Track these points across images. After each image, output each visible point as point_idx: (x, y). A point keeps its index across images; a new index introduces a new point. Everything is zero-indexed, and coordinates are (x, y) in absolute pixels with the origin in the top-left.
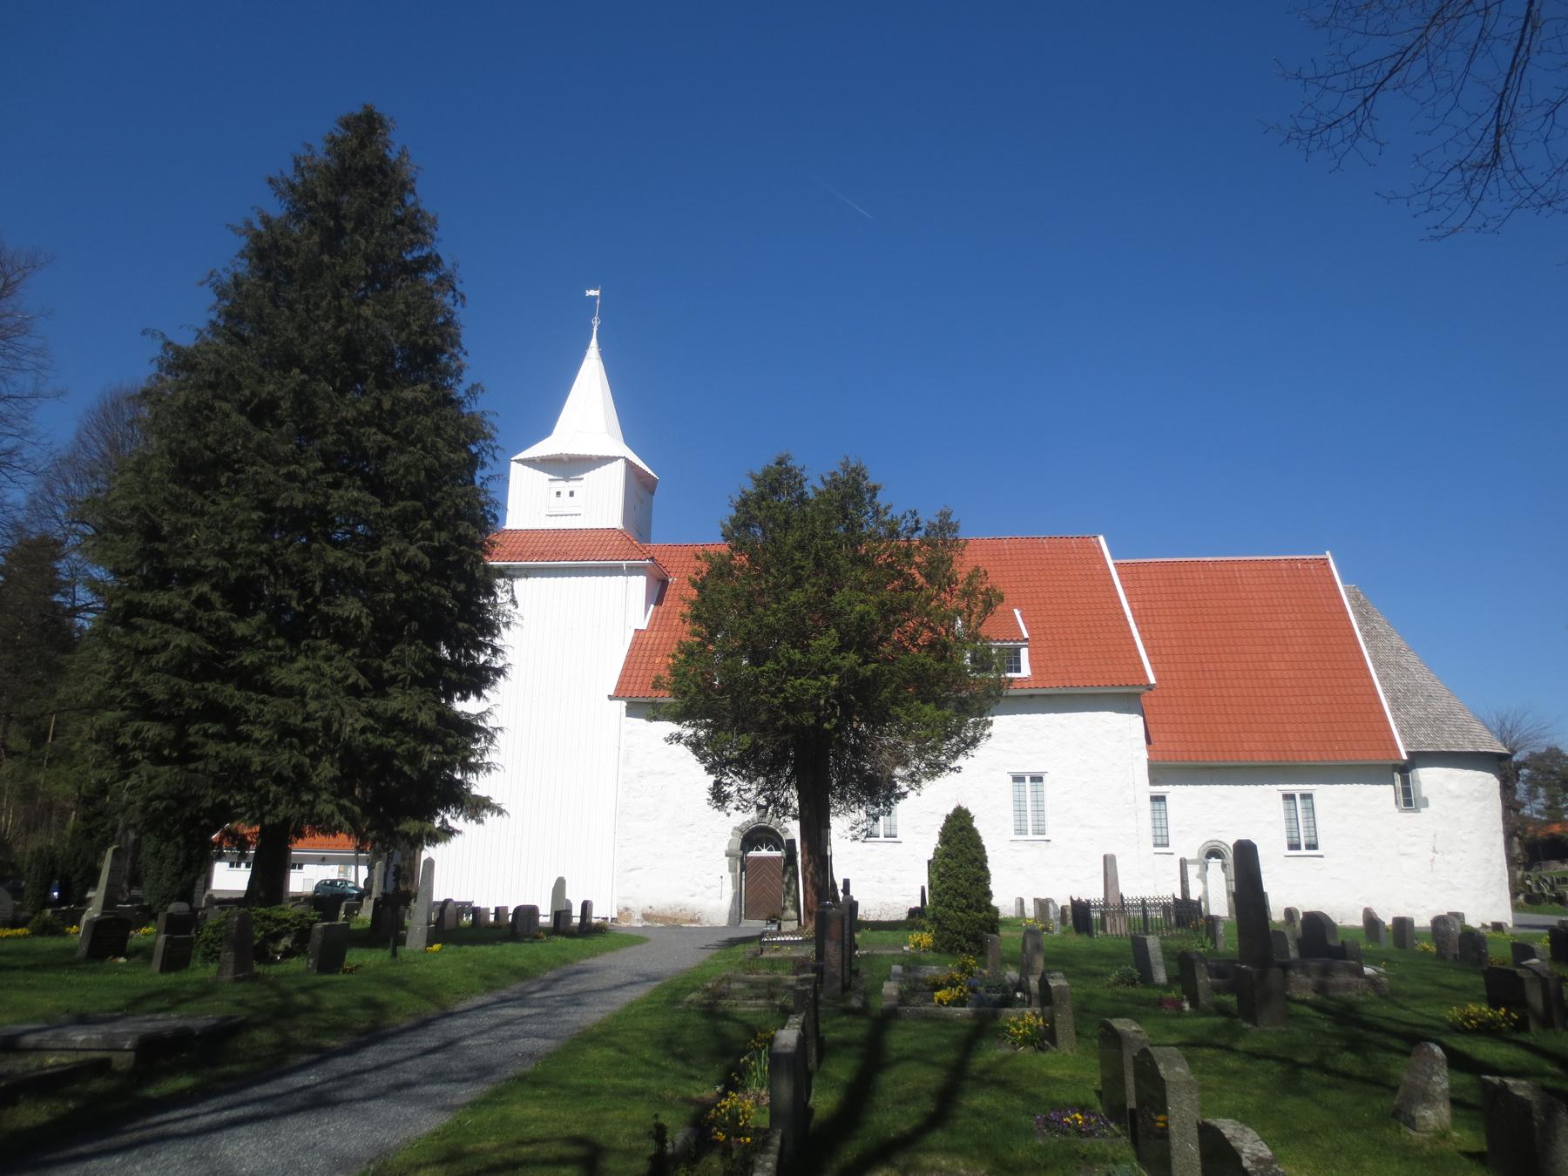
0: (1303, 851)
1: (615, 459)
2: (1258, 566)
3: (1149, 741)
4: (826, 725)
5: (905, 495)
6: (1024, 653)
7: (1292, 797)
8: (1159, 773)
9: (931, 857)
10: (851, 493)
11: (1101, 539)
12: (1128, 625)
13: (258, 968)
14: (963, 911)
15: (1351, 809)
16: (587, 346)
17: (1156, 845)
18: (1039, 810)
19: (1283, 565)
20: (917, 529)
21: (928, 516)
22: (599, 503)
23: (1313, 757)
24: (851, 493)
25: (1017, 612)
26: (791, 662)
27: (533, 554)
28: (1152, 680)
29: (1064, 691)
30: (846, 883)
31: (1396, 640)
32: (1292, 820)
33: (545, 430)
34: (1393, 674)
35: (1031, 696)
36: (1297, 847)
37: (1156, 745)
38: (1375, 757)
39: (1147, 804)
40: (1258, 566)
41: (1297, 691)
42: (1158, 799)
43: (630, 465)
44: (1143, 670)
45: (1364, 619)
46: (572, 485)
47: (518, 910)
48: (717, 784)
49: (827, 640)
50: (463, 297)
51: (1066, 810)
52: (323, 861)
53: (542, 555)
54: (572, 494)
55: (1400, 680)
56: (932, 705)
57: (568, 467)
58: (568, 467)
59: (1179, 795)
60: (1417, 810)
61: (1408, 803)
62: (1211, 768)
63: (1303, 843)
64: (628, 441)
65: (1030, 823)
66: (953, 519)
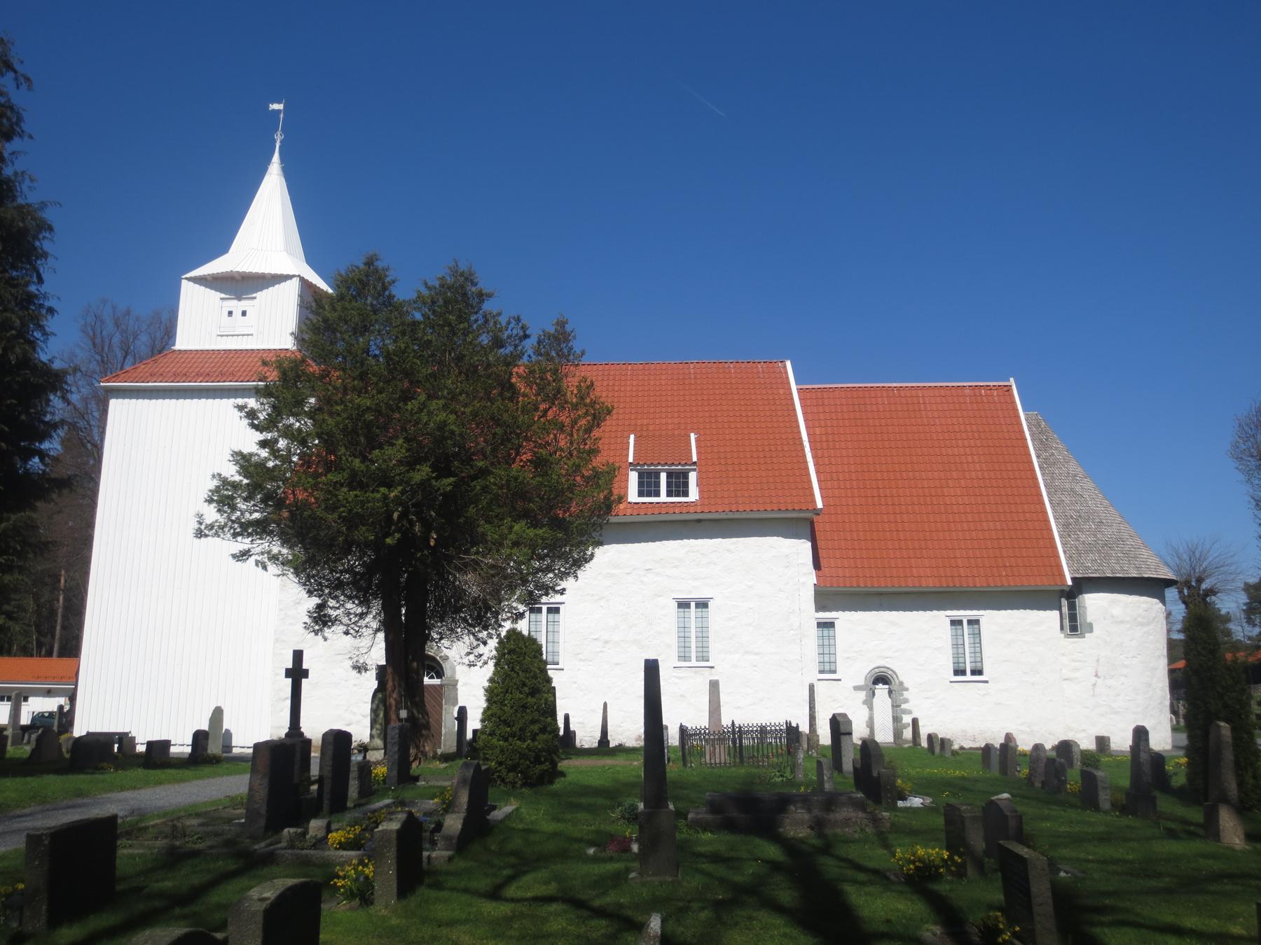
0: (969, 677)
1: (294, 276)
2: (943, 392)
3: (817, 565)
4: (389, 541)
5: (520, 301)
6: (693, 477)
7: (960, 623)
8: (826, 598)
9: (487, 684)
10: (457, 300)
11: (788, 364)
12: (803, 450)
13: (900, 804)
14: (506, 740)
15: (1018, 636)
16: (268, 161)
17: (821, 672)
18: (703, 637)
19: (967, 391)
20: (526, 336)
21: (540, 325)
22: (273, 324)
23: (980, 584)
24: (457, 300)
25: (693, 436)
26: (354, 474)
27: (222, 374)
28: (820, 505)
29: (730, 516)
30: (567, 718)
31: (1073, 467)
32: (957, 646)
33: (222, 246)
34: (1067, 500)
35: (699, 521)
36: (963, 673)
37: (825, 570)
38: (1045, 583)
39: (813, 631)
40: (943, 392)
41: (970, 517)
42: (827, 625)
43: (305, 284)
44: (812, 495)
45: (1042, 446)
46: (244, 304)
47: (150, 744)
48: (320, 607)
49: (395, 452)
50: (28, 79)
51: (683, 633)
52: (49, 693)
53: (207, 376)
54: (244, 313)
55: (1071, 504)
56: (523, 523)
57: (241, 285)
58: (241, 285)
59: (848, 622)
60: (1082, 636)
61: (1074, 628)
62: (881, 594)
63: (968, 670)
64: (311, 260)
65: (693, 649)
66: (568, 328)
